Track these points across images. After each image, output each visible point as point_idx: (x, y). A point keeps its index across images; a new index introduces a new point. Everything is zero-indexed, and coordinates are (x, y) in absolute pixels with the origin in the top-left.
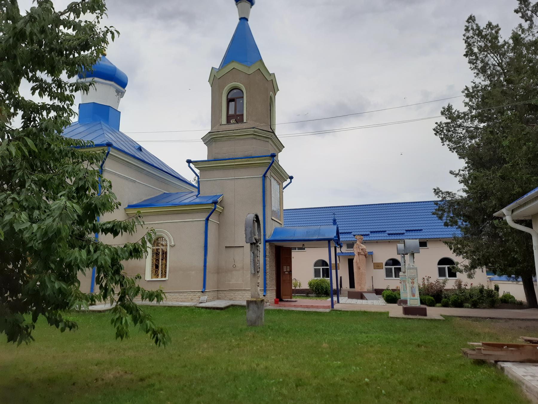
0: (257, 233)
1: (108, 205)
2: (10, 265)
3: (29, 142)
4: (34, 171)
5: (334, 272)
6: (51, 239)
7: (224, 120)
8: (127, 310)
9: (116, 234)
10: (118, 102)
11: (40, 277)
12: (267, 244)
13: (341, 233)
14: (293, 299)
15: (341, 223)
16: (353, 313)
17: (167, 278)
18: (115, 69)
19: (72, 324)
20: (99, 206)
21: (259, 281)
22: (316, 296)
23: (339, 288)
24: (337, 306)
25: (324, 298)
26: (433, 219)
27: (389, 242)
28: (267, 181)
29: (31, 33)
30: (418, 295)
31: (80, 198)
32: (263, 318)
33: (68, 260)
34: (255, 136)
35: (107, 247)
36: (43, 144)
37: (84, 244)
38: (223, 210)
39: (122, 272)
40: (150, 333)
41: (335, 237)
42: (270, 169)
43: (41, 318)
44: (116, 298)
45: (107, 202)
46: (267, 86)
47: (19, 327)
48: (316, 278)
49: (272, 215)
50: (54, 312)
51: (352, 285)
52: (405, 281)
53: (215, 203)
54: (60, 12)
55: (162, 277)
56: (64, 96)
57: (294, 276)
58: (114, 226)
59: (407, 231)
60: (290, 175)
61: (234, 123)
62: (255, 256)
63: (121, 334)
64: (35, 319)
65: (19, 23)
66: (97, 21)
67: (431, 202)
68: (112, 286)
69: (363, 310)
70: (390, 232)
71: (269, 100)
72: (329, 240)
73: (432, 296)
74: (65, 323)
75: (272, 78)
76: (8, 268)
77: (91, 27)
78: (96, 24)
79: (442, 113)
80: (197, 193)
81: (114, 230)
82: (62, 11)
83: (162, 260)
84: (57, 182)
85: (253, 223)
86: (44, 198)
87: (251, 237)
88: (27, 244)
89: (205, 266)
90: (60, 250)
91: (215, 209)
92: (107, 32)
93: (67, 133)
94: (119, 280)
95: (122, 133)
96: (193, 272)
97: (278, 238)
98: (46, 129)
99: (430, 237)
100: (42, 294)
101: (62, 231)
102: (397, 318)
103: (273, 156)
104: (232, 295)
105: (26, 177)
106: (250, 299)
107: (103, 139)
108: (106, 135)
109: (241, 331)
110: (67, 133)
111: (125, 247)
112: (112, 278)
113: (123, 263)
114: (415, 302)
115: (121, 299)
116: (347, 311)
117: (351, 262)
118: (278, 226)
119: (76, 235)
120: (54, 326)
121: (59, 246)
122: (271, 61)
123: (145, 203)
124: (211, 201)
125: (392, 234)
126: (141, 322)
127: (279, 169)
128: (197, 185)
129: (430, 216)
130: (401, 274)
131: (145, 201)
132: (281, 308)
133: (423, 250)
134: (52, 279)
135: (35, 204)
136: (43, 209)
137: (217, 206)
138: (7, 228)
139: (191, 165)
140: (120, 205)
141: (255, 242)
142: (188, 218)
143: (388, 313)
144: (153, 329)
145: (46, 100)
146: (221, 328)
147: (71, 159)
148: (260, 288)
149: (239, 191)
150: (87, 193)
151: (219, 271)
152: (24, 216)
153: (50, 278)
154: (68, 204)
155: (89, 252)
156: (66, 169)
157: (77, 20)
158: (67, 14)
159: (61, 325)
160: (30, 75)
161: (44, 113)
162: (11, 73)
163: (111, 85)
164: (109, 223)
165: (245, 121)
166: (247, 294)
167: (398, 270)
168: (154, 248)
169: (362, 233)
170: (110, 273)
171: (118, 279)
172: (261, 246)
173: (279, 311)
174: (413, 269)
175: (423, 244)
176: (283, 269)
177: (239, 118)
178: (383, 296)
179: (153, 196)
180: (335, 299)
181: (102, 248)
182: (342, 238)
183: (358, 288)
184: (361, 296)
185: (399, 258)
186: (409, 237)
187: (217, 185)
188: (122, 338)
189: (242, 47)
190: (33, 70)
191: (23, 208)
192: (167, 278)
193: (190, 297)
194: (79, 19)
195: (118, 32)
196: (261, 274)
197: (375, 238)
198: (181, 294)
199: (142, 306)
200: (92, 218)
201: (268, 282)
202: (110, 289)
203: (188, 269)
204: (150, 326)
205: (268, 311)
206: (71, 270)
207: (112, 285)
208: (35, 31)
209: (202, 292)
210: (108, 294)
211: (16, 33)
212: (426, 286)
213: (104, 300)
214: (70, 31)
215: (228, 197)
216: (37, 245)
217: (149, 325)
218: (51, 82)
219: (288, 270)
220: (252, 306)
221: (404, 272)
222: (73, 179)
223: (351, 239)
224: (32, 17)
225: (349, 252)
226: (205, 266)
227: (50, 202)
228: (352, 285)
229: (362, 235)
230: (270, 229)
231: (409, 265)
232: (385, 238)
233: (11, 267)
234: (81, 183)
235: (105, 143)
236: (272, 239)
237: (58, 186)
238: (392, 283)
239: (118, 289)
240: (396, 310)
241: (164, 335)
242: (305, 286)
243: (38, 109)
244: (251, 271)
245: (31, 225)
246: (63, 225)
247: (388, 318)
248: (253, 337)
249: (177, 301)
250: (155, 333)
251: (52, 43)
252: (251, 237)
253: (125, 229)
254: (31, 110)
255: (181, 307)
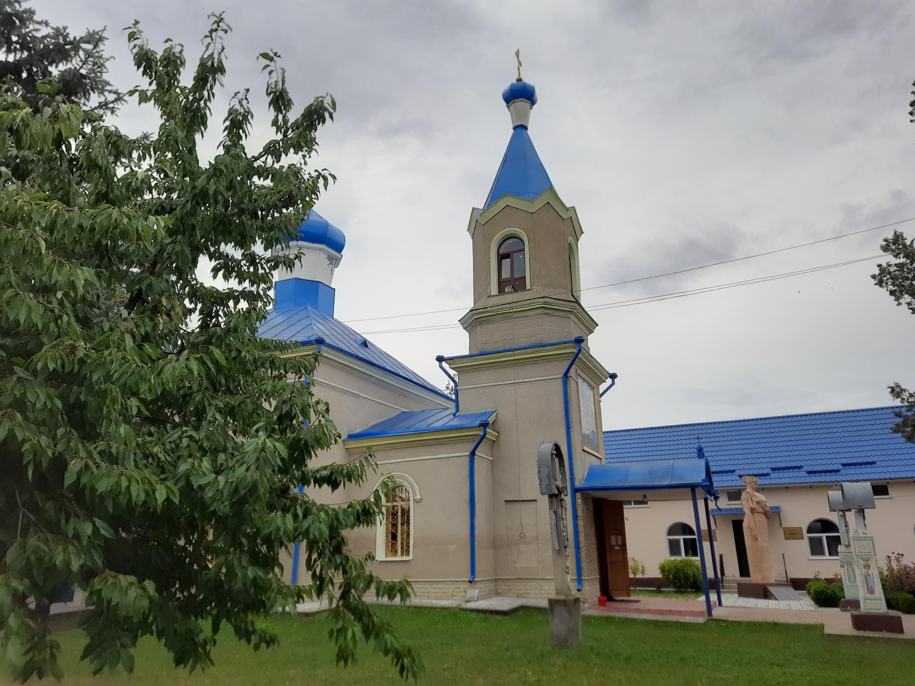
0: (559, 477)
1: (323, 441)
2: (180, 539)
3: (217, 352)
4: (216, 391)
5: (706, 545)
6: (242, 498)
7: (494, 289)
8: (354, 614)
9: (334, 485)
10: (332, 274)
11: (226, 559)
12: (578, 495)
13: (714, 473)
14: (633, 598)
15: (713, 454)
16: (753, 627)
17: (411, 557)
18: (326, 225)
19: (271, 637)
20: (311, 442)
21: (568, 564)
22: (676, 592)
23: (719, 576)
24: (717, 612)
25: (692, 596)
26: (896, 441)
27: (811, 487)
28: (572, 383)
29: (216, 192)
30: (882, 591)
31: (283, 431)
32: (581, 634)
33: (266, 531)
34: (548, 309)
35: (322, 508)
36: (230, 351)
37: (288, 504)
38: (497, 437)
39: (344, 549)
40: (391, 655)
41: (704, 481)
42: (576, 363)
43: (226, 627)
44: (337, 593)
45: (322, 435)
46: (564, 228)
47: (195, 642)
48: (673, 558)
49: (583, 443)
50: (242, 615)
51: (744, 570)
52: (850, 564)
53: (485, 425)
54: (253, 157)
55: (402, 555)
56: (258, 277)
57: (630, 555)
58: (332, 473)
59: (844, 465)
60: (611, 372)
61: (511, 293)
62: (558, 518)
63: (343, 656)
64: (216, 629)
65: (200, 180)
66: (303, 162)
67: (887, 408)
68: (330, 575)
69: (770, 619)
70: (810, 469)
71: (567, 251)
72: (693, 487)
73: (910, 593)
74: (260, 635)
75: (571, 213)
76: (177, 545)
77: (295, 171)
78: (303, 166)
79: (886, 249)
80: (454, 410)
81: (332, 480)
82: (256, 155)
83: (402, 524)
84: (250, 407)
85: (552, 459)
86: (231, 433)
87: (550, 484)
88: (209, 507)
89: (472, 535)
90: (255, 516)
91: (485, 435)
92: (318, 177)
93: (266, 331)
94: (341, 563)
95: (339, 323)
96: (453, 547)
97: (597, 483)
98: (236, 330)
99: (893, 476)
100: (226, 587)
101: (259, 485)
102: (841, 636)
103: (579, 341)
104: (522, 587)
105: (206, 403)
106: (554, 596)
107: (310, 334)
108: (314, 327)
109: (542, 655)
110: (266, 331)
111: (349, 507)
112: (330, 560)
113: (345, 533)
114: (874, 603)
115: (345, 595)
116: (740, 623)
117: (738, 527)
118: (595, 462)
119: (276, 489)
120: (243, 641)
121: (255, 510)
122: (567, 183)
123: (375, 430)
124: (477, 423)
125: (815, 472)
126: (377, 637)
127: (592, 363)
128: (454, 397)
129: (888, 436)
130: (840, 548)
131: (374, 426)
132: (612, 614)
133: (880, 501)
134: (244, 563)
135: (220, 443)
136: (230, 450)
137: (488, 430)
138: (182, 483)
139: (444, 364)
140: (340, 437)
141: (557, 492)
142: (442, 453)
143: (822, 626)
144: (396, 650)
145: (233, 284)
146: (507, 650)
147: (269, 371)
148: (571, 577)
149: (523, 404)
150: (294, 422)
151: (496, 544)
152: (206, 464)
153: (240, 562)
154: (269, 443)
155: (296, 517)
156: (263, 388)
157: (277, 166)
158: (263, 159)
159: (254, 639)
160: (212, 249)
161: (231, 304)
162: (187, 251)
163: (320, 250)
164: (325, 468)
165: (528, 287)
166: (547, 587)
167: (834, 543)
168: (390, 504)
169: (756, 472)
170: (327, 551)
171: (338, 561)
172: (568, 499)
173: (609, 620)
174: (865, 539)
175: (880, 490)
176: (610, 542)
177: (518, 284)
178: (809, 593)
179: (386, 419)
180: (713, 597)
181: (314, 510)
182: (718, 482)
183: (755, 577)
184: (763, 592)
185: (834, 517)
186: (850, 478)
187: (488, 396)
188: (346, 663)
189: (521, 170)
190: (217, 243)
191: (204, 452)
192: (411, 557)
193: (450, 590)
194: (280, 164)
195: (334, 177)
196: (571, 550)
197: (782, 481)
198: (435, 586)
199: (373, 605)
200: (301, 463)
201: (584, 565)
202: (327, 579)
203: (447, 543)
204: (392, 642)
205: (588, 619)
206: (271, 548)
207: (331, 572)
208: (222, 188)
209: (470, 582)
210: (324, 587)
211: (195, 195)
212: (895, 571)
213: (318, 597)
214: (268, 183)
215: (506, 415)
216: (224, 508)
217: (389, 643)
218: (240, 258)
219: (620, 542)
220: (558, 609)
221: (848, 546)
222: (274, 403)
223: (734, 484)
224: (216, 169)
225: (733, 507)
226: (472, 535)
227: (240, 439)
228: (744, 570)
229: (756, 475)
230: (582, 469)
231: (856, 531)
232: (802, 480)
233: (181, 542)
234: (285, 409)
235: (313, 338)
236: (586, 485)
237: (251, 414)
238: (825, 567)
239: (339, 579)
240: (837, 622)
241: (413, 660)
242: (654, 573)
243: (222, 298)
244: (553, 545)
245: (216, 477)
246: (261, 476)
247: (823, 635)
248: (565, 667)
249: (428, 598)
250: (398, 656)
251: (242, 202)
252: (550, 484)
253: (349, 477)
254: (211, 301)
255: (435, 608)
